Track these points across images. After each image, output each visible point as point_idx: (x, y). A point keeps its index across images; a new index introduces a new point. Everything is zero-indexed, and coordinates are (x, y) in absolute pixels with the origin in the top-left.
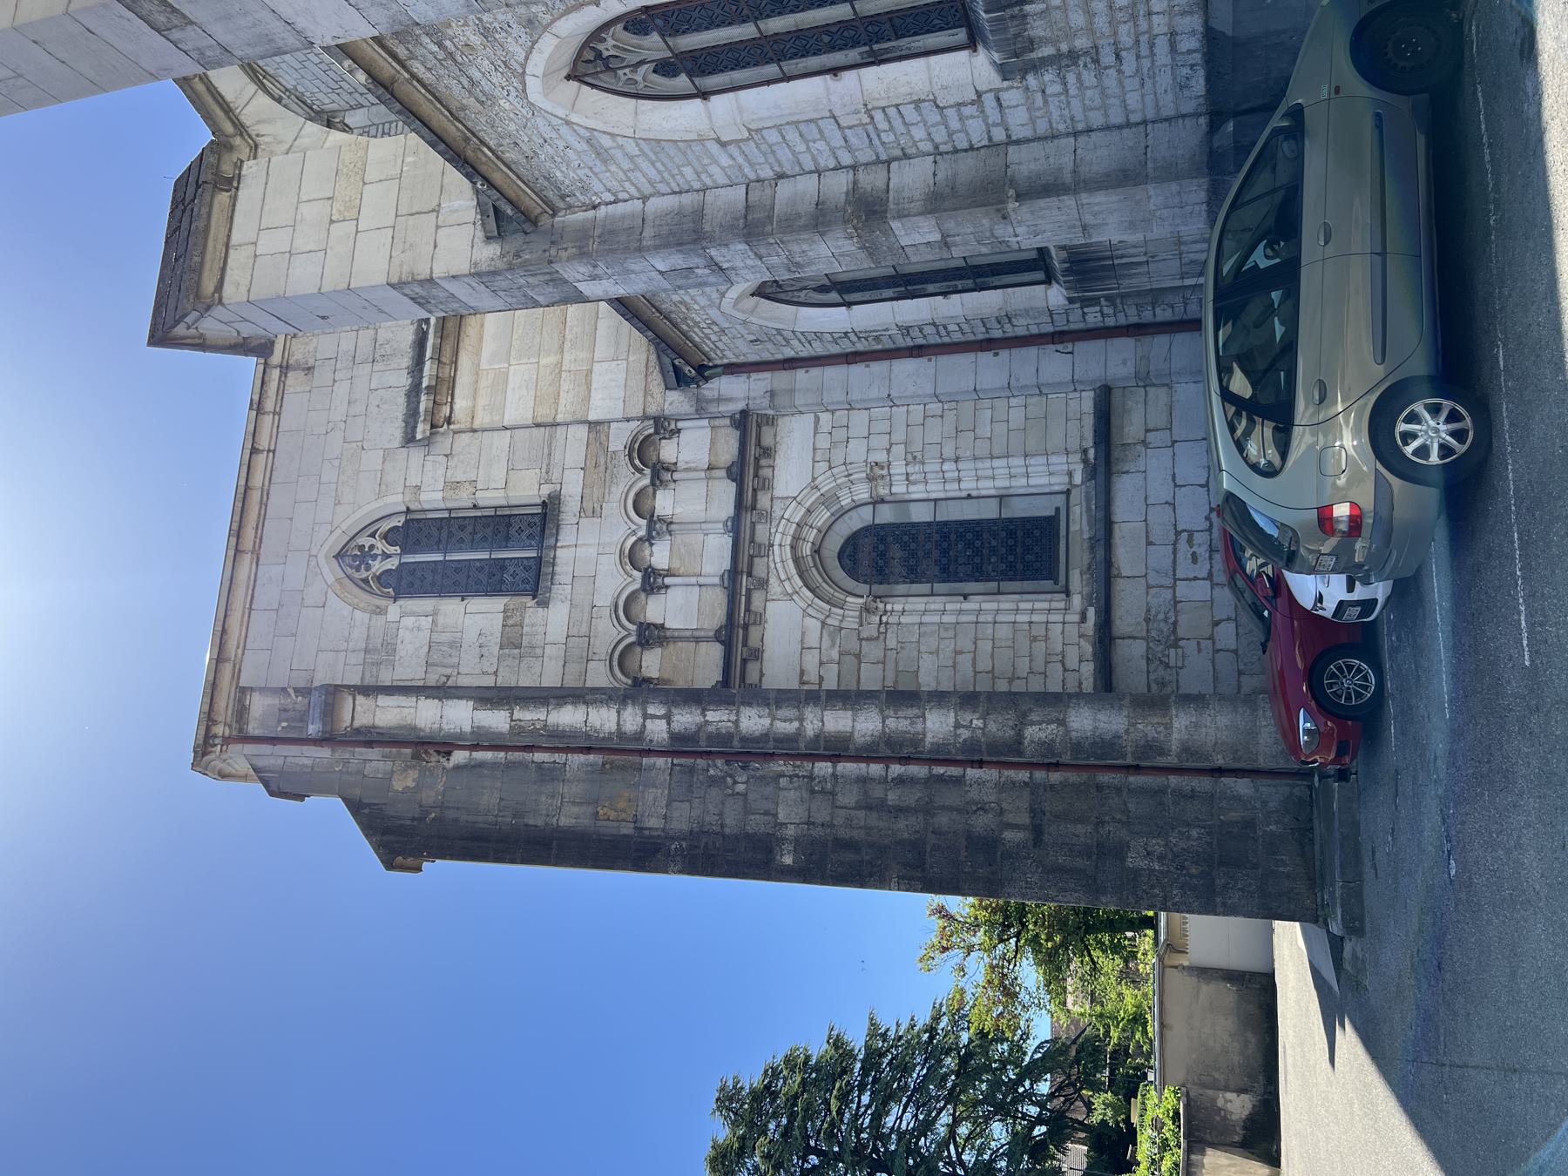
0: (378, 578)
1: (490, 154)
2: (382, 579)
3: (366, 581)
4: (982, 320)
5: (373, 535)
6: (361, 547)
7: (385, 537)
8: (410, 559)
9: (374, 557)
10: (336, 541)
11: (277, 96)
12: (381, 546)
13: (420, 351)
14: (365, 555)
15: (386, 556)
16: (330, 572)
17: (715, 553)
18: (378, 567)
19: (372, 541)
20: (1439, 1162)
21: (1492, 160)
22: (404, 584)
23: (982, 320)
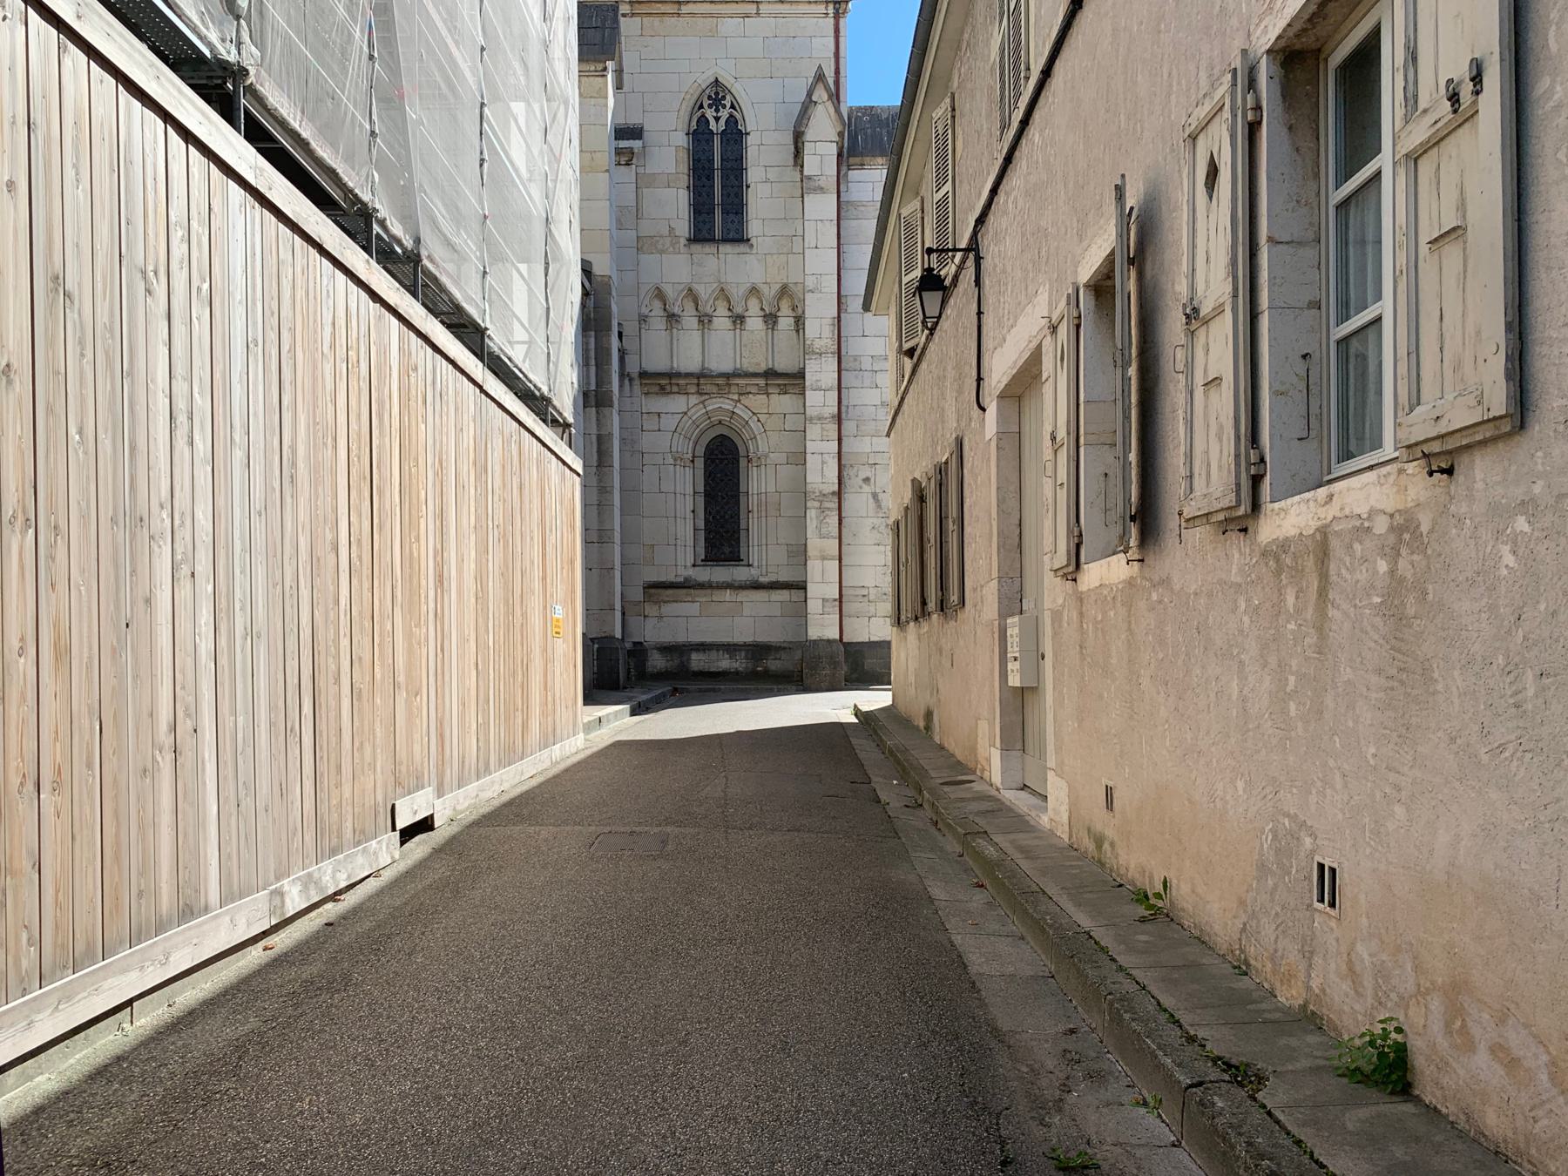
0: (703, 116)
1: (515, 453)
2: (703, 120)
3: (701, 107)
4: (1036, 688)
5: (733, 107)
6: (724, 98)
7: (731, 116)
8: (717, 141)
9: (717, 110)
10: (727, 80)
11: (129, 378)
12: (724, 114)
13: (1053, 54)
14: (717, 102)
15: (717, 119)
16: (705, 79)
17: (721, 362)
18: (710, 114)
19: (728, 105)
20: (736, 517)
21: (994, 633)
22: (700, 134)
23: (1036, 688)
